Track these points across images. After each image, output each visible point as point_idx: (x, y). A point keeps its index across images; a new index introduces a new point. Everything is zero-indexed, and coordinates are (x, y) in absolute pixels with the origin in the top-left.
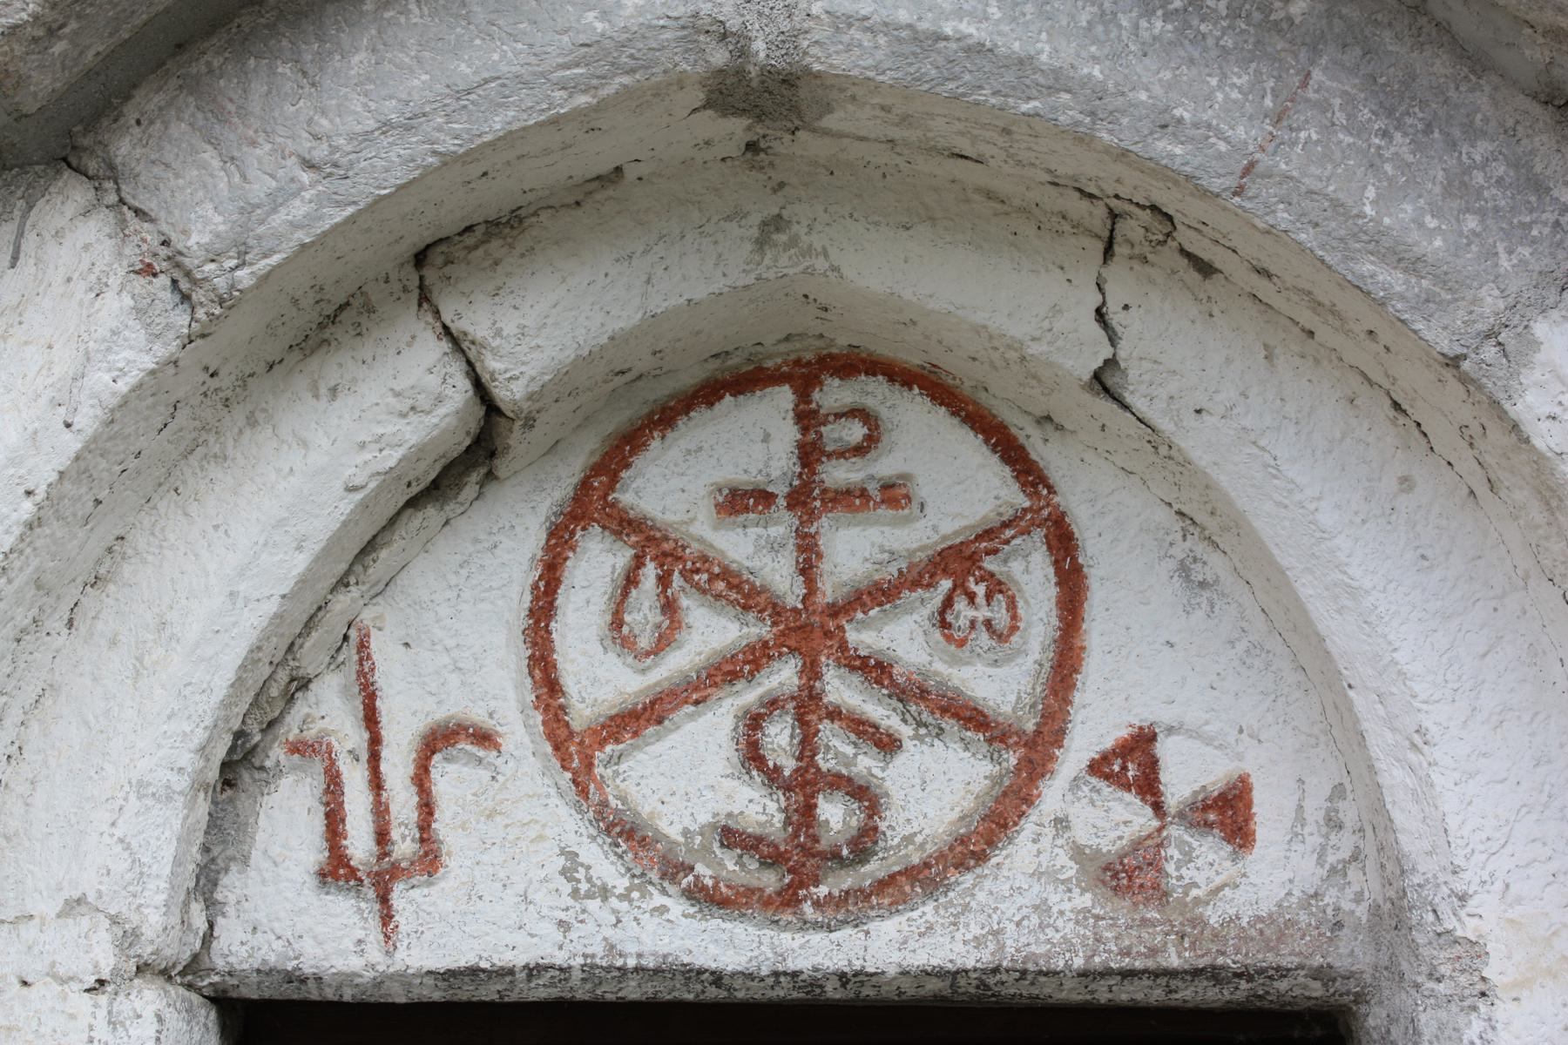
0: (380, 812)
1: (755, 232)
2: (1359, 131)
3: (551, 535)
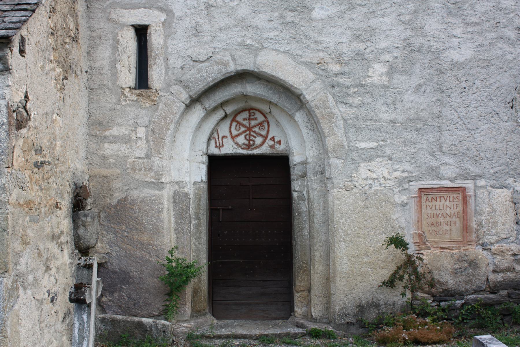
0: (219, 142)
2: (285, 99)
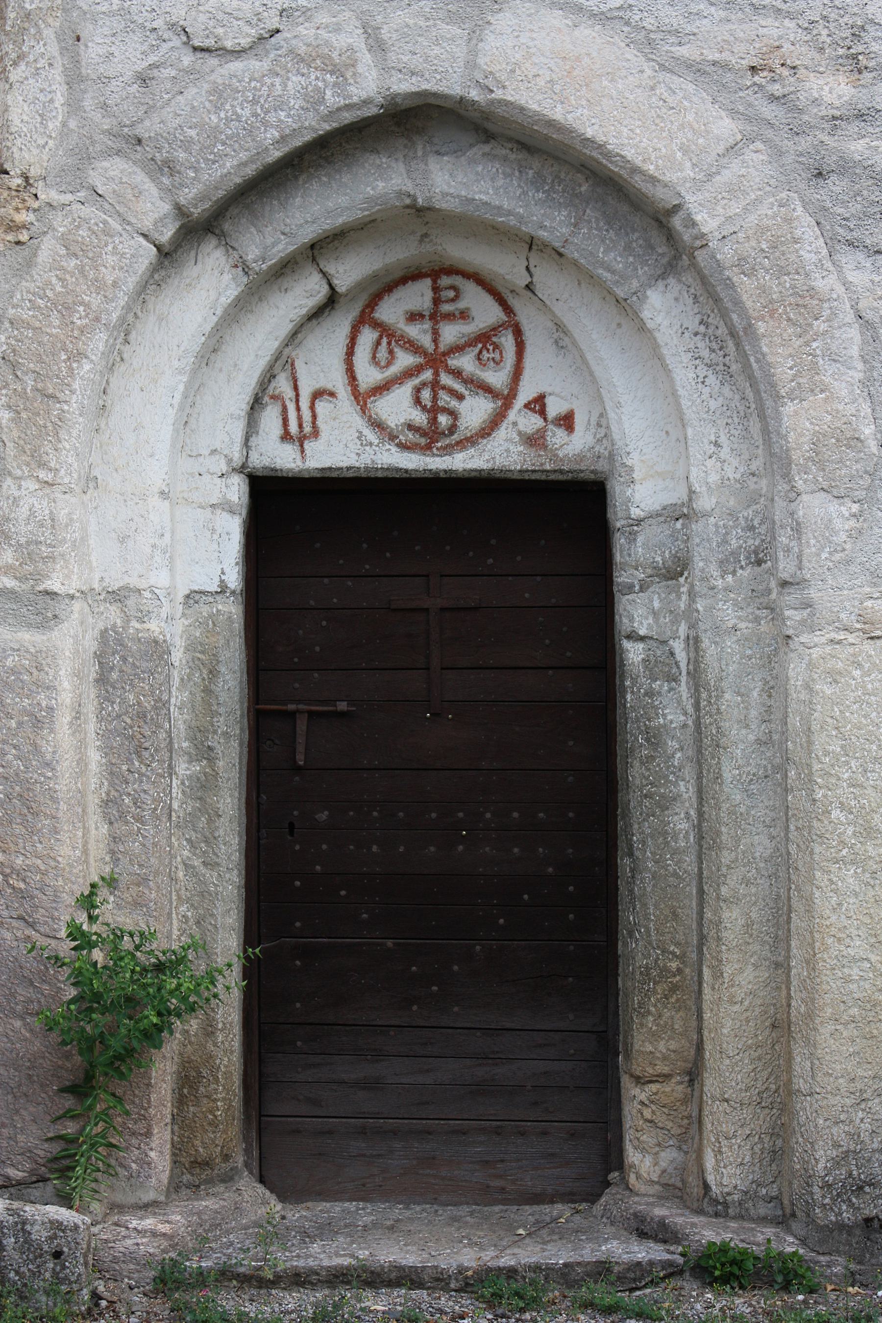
0: (300, 418)
1: (419, 238)
3: (352, 328)
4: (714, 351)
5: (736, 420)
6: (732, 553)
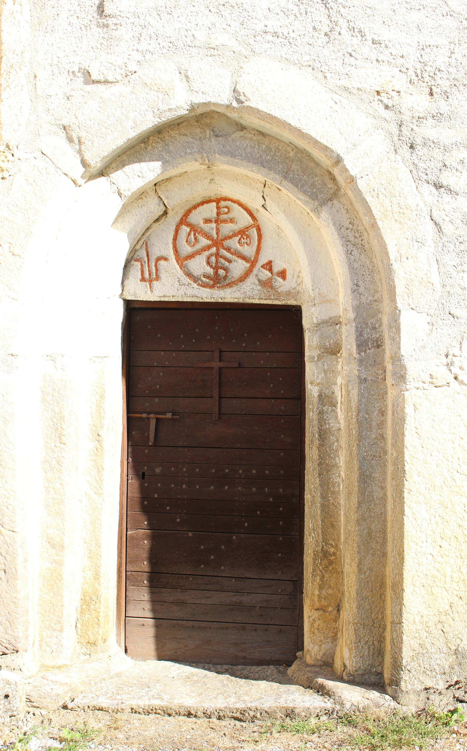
0: (149, 271)
3: (176, 226)
4: (356, 238)
5: (367, 273)
6: (364, 341)
